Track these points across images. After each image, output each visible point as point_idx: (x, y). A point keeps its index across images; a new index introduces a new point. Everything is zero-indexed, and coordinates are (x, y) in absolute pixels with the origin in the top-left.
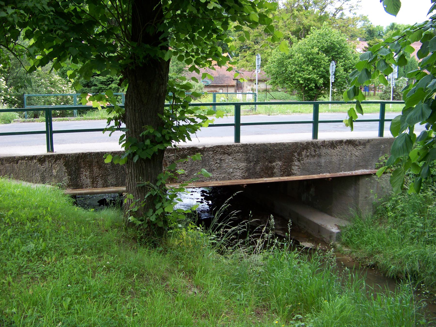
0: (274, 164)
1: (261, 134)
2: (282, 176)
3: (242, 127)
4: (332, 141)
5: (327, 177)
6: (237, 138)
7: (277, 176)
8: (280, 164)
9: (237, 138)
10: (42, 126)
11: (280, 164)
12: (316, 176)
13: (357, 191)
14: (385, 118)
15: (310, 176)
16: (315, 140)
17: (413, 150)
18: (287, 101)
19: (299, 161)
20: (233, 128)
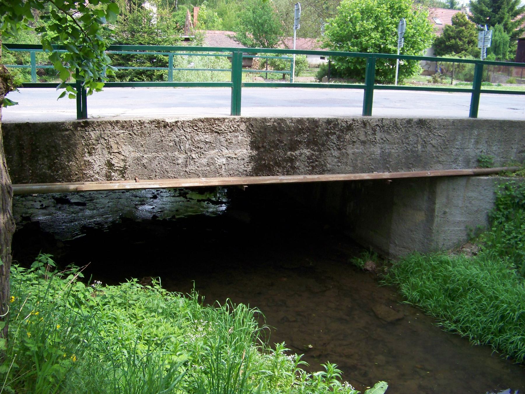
0: (297, 152)
1: (273, 106)
2: (311, 173)
3: (482, 95)
4: (395, 120)
5: (384, 177)
6: (236, 107)
7: (302, 173)
8: (308, 153)
9: (236, 107)
10: (227, 77)
11: (308, 153)
12: (366, 176)
13: (432, 201)
14: (470, 94)
15: (357, 175)
16: (367, 117)
17: (443, 23)
18: (414, 86)
19: (339, 149)
20: (228, 91)
